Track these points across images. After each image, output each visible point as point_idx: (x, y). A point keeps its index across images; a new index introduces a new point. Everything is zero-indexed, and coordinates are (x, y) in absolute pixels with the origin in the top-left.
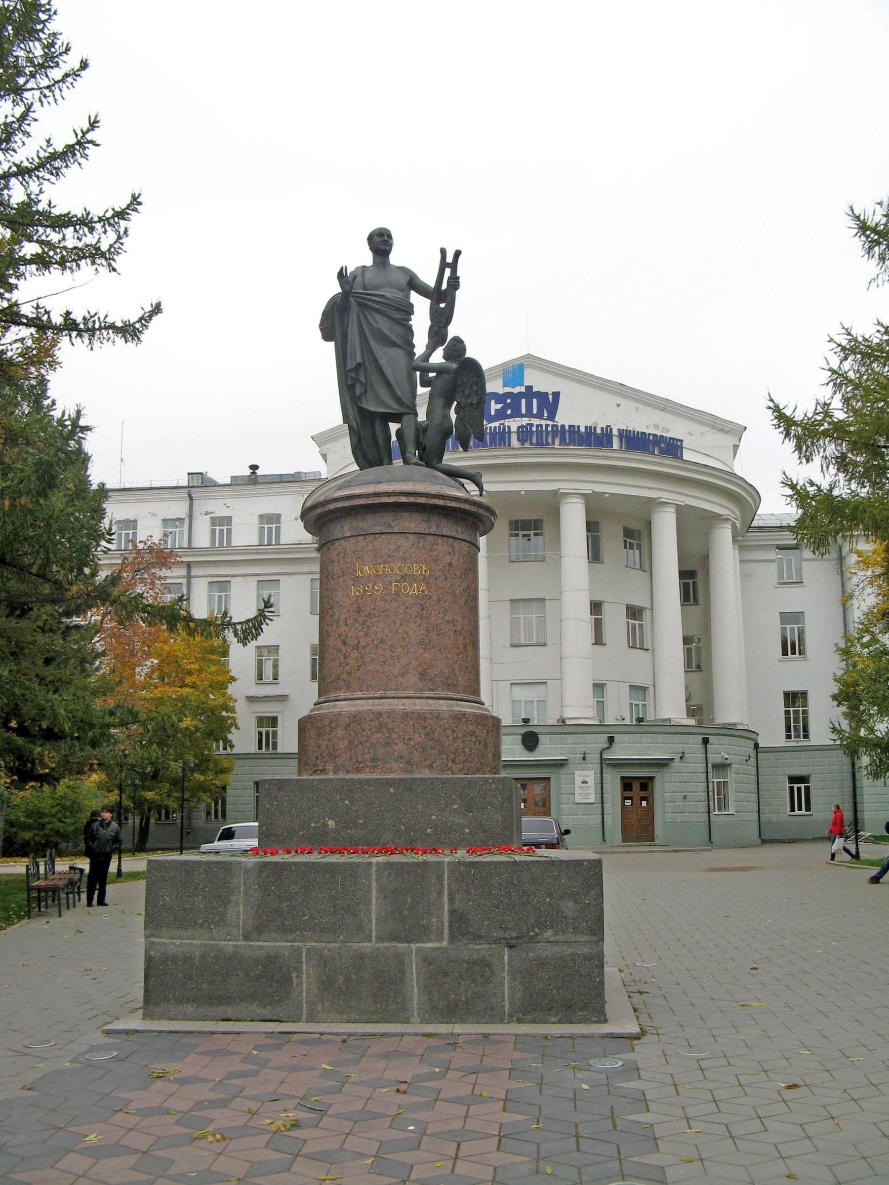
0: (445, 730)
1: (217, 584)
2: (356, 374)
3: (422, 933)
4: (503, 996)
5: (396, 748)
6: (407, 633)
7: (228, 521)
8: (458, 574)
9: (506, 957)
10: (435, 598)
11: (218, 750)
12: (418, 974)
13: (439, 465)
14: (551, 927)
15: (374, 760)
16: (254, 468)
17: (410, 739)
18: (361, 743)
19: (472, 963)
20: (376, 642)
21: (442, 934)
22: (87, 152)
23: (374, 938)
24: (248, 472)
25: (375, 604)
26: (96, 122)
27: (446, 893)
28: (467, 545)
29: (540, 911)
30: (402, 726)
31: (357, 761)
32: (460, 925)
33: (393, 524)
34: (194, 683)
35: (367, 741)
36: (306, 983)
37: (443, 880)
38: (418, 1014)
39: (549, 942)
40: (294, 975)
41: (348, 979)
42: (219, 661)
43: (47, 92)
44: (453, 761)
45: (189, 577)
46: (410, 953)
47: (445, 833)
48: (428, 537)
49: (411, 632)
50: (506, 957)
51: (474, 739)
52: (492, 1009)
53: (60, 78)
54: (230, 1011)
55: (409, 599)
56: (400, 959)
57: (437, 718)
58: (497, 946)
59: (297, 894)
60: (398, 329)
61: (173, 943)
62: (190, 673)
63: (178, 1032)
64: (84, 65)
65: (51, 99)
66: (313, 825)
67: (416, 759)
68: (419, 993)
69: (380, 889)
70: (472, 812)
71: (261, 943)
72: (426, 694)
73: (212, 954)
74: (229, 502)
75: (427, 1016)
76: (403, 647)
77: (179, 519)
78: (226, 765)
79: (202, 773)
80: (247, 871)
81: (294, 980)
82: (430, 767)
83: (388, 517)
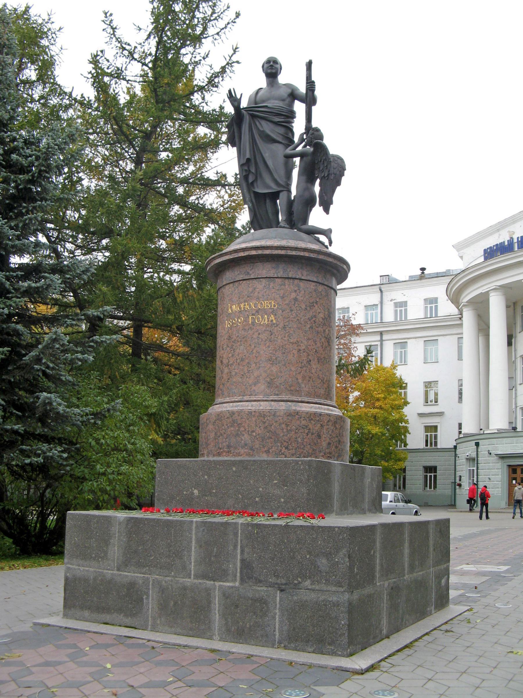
0: (280, 424)
1: (399, 344)
2: (248, 168)
3: (221, 575)
4: (275, 628)
5: (243, 438)
6: (259, 353)
7: (404, 304)
8: (303, 307)
9: (278, 598)
10: (281, 325)
11: (400, 447)
12: (219, 604)
13: (304, 227)
14: (310, 578)
15: (229, 446)
16: (423, 269)
17: (253, 431)
18: (221, 435)
19: (255, 600)
20: (238, 361)
21: (235, 576)
22: (233, 69)
23: (192, 576)
24: (420, 272)
25: (238, 333)
26: (237, 48)
27: (239, 547)
28: (314, 284)
29: (302, 565)
30: (247, 421)
31: (219, 448)
32: (248, 572)
33: (251, 272)
34: (381, 406)
35: (225, 433)
36: (151, 603)
37: (237, 537)
38: (219, 634)
39: (308, 589)
40: (145, 597)
41: (176, 603)
42: (397, 392)
43: (216, 37)
44: (287, 448)
45: (382, 341)
46: (215, 589)
47: (268, 501)
48: (277, 280)
49: (262, 352)
50: (278, 598)
51: (307, 431)
52: (267, 636)
53: (224, 26)
54: (108, 617)
55: (261, 327)
56: (208, 591)
57: (274, 415)
58: (272, 589)
59: (147, 541)
60: (282, 130)
61: (79, 569)
62: (378, 400)
63: (70, 628)
64: (238, 15)
65: (220, 40)
66: (185, 493)
67: (257, 446)
68: (219, 619)
69: (198, 541)
70: (286, 486)
71: (126, 574)
72: (271, 398)
73: (100, 578)
74: (405, 292)
75: (224, 636)
76: (256, 363)
77: (374, 305)
78: (403, 456)
79: (387, 461)
80: (120, 524)
81: (145, 601)
82: (268, 452)
83: (247, 268)
